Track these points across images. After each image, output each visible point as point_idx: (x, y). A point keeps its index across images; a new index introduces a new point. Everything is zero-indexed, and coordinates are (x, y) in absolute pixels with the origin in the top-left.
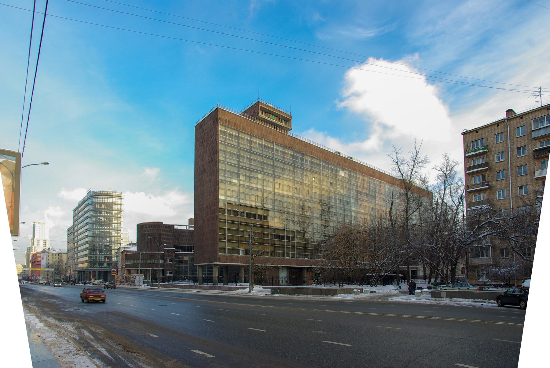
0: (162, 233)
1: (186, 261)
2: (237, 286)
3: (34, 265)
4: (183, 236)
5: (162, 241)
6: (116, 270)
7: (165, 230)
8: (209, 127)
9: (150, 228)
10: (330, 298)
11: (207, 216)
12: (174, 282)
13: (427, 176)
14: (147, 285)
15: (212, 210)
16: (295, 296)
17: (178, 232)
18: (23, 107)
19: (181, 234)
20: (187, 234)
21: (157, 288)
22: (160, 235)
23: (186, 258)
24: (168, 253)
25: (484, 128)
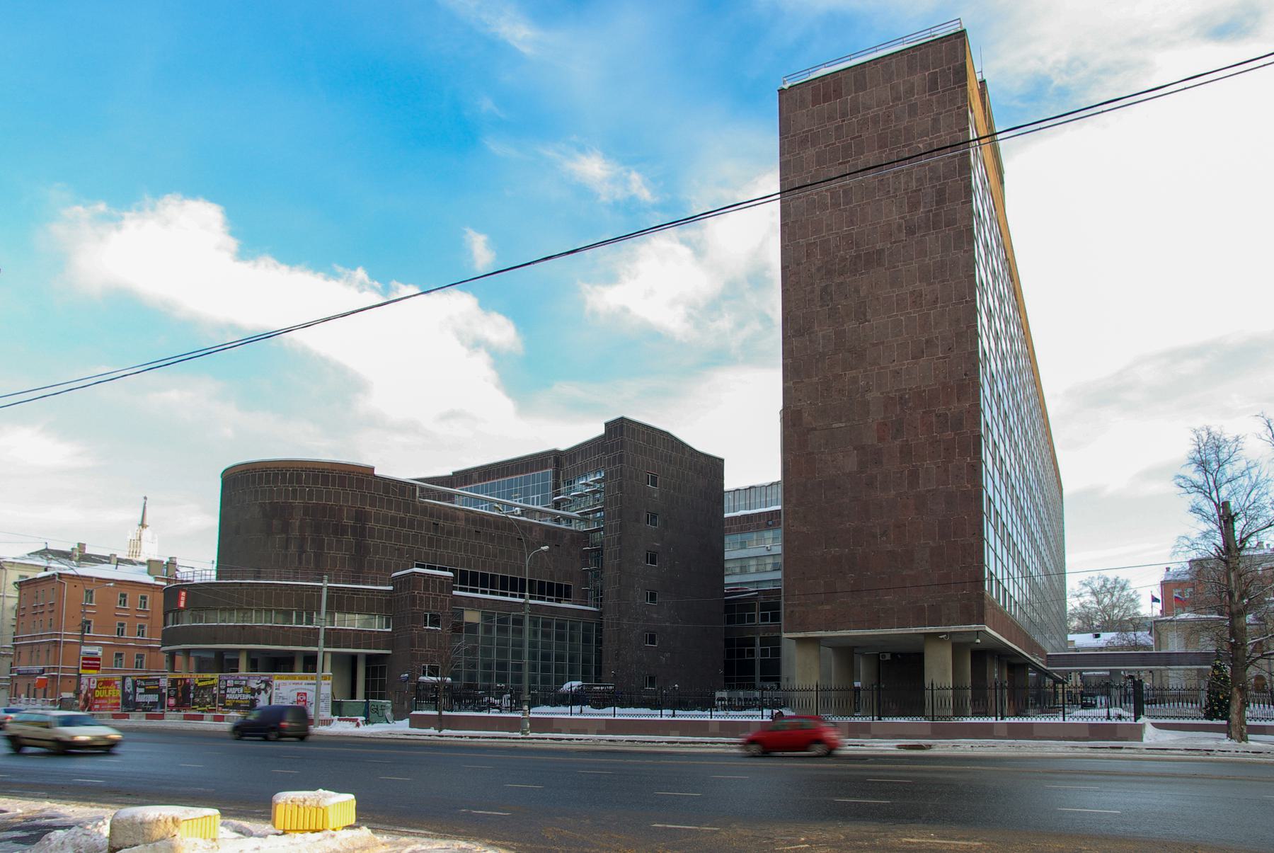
0: (368, 508)
1: (472, 627)
2: (573, 717)
3: (862, 666)
4: (449, 533)
5: (370, 541)
6: (100, 653)
7: (381, 500)
8: (897, 99)
9: (315, 482)
10: (547, 739)
11: (895, 438)
12: (677, 712)
13: (1199, 532)
14: (367, 722)
15: (938, 416)
16: (515, 733)
17: (432, 515)
18: (1186, 88)
19: (441, 523)
20: (461, 524)
21: (518, 735)
22: (361, 516)
23: (472, 617)
24: (426, 588)
25: (728, 756)
